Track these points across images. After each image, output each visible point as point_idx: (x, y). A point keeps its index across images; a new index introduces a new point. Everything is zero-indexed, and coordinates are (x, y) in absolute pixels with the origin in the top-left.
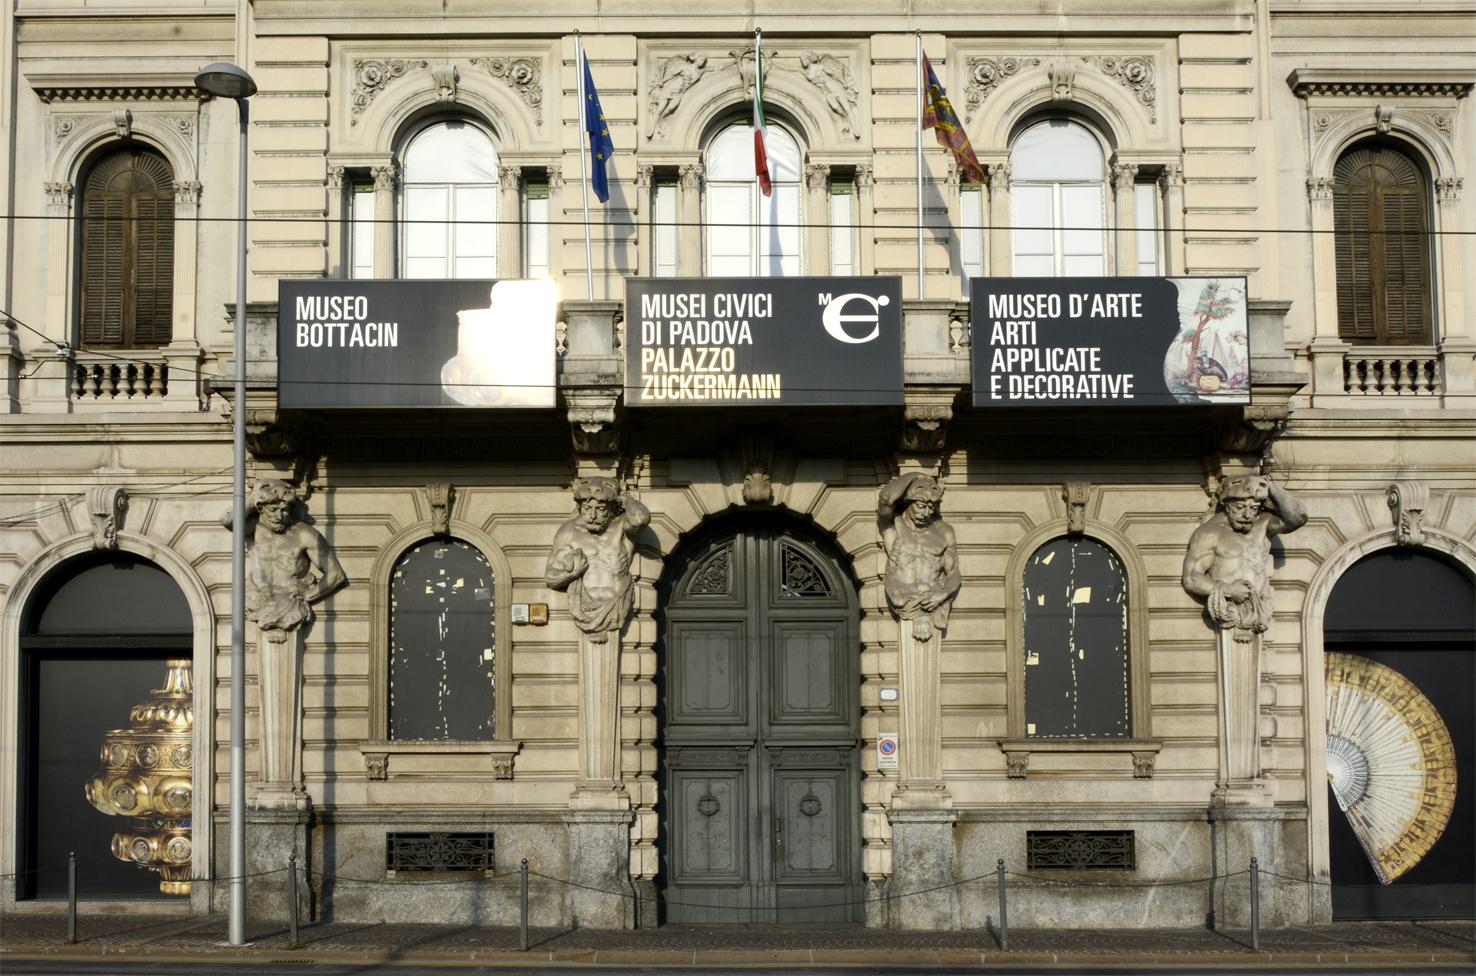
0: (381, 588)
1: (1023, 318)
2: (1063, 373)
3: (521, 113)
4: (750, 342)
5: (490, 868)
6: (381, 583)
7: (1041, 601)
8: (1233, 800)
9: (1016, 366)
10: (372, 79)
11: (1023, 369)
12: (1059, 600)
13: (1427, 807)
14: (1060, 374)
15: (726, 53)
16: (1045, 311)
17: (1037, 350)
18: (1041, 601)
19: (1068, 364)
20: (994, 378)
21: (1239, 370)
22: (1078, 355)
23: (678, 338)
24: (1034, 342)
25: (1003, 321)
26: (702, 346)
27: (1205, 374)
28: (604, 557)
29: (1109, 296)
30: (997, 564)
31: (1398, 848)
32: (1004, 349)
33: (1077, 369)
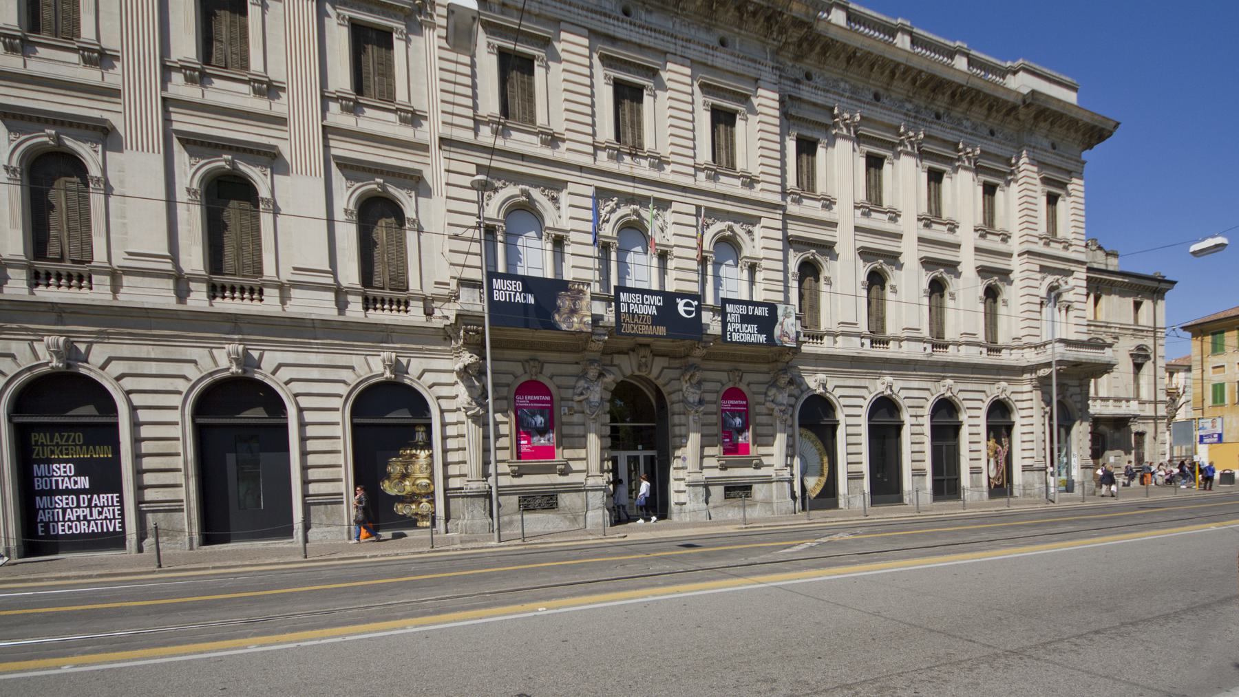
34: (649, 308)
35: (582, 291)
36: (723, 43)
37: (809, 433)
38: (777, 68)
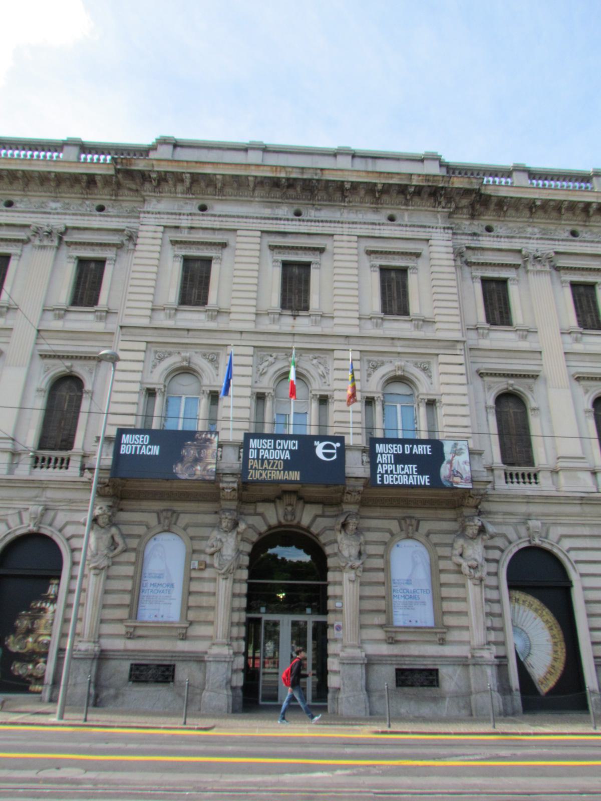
1: (388, 453)
9: (386, 471)
13: (555, 659)
14: (403, 475)
16: (396, 451)
20: (378, 475)
23: (263, 456)
25: (381, 454)
29: (406, 446)
31: (546, 678)
32: (382, 464)
34: (283, 452)
35: (209, 440)
36: (391, 219)
37: (530, 598)
38: (448, 228)
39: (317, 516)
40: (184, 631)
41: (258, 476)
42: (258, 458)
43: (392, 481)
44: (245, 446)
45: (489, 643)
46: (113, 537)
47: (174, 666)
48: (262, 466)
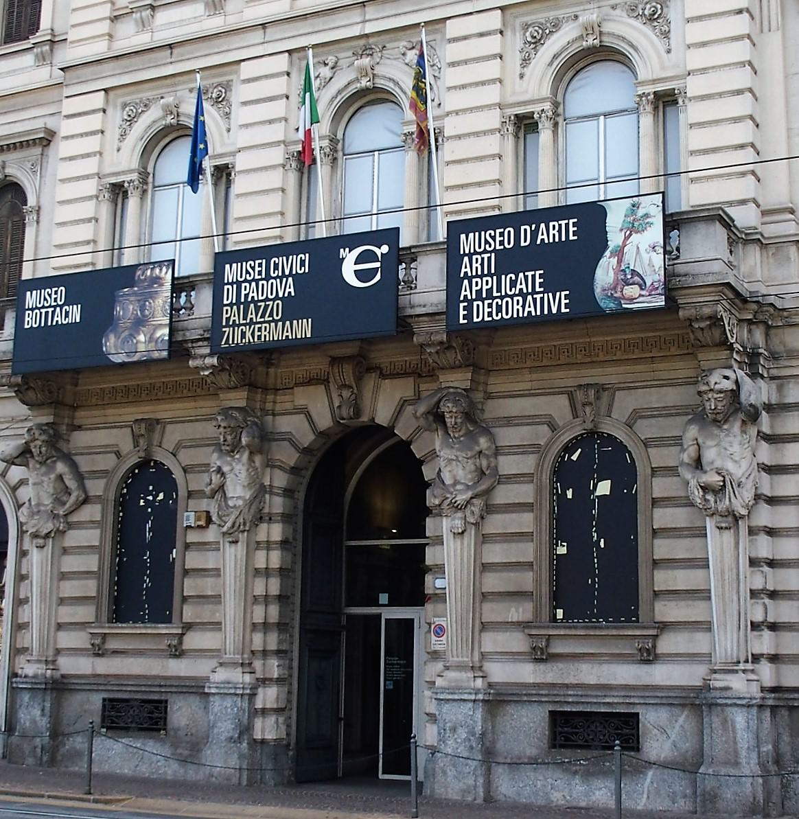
0: (110, 503)
1: (485, 251)
2: (515, 295)
3: (652, 43)
4: (293, 294)
5: (164, 729)
6: (110, 498)
7: (570, 494)
8: (718, 684)
9: (479, 292)
10: (129, 116)
11: (484, 296)
12: (584, 492)
14: (512, 297)
15: (350, 54)
16: (502, 243)
17: (495, 278)
18: (570, 494)
19: (519, 287)
20: (462, 305)
21: (656, 278)
22: (526, 278)
23: (247, 296)
24: (493, 271)
25: (470, 255)
26: (262, 301)
27: (628, 285)
28: (237, 472)
29: (551, 224)
30: (526, 464)
32: (470, 279)
33: (525, 291)
39: (404, 403)
40: (175, 642)
41: (238, 339)
42: (238, 303)
43: (490, 314)
44: (216, 280)
45: (756, 658)
46: (60, 478)
47: (166, 701)
48: (245, 319)
